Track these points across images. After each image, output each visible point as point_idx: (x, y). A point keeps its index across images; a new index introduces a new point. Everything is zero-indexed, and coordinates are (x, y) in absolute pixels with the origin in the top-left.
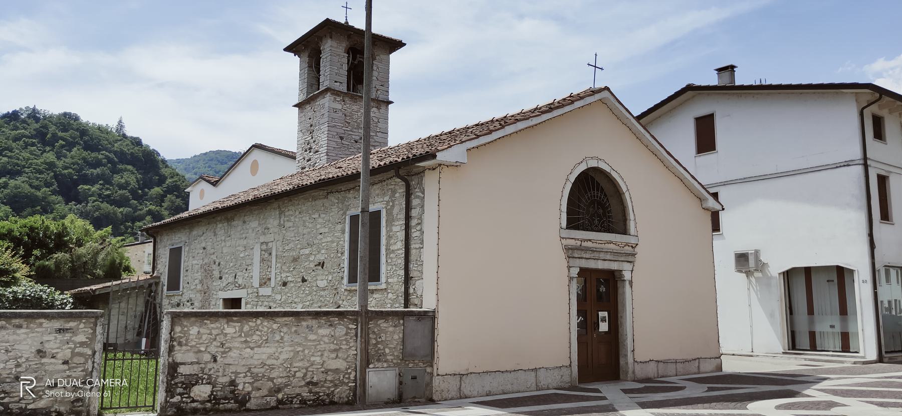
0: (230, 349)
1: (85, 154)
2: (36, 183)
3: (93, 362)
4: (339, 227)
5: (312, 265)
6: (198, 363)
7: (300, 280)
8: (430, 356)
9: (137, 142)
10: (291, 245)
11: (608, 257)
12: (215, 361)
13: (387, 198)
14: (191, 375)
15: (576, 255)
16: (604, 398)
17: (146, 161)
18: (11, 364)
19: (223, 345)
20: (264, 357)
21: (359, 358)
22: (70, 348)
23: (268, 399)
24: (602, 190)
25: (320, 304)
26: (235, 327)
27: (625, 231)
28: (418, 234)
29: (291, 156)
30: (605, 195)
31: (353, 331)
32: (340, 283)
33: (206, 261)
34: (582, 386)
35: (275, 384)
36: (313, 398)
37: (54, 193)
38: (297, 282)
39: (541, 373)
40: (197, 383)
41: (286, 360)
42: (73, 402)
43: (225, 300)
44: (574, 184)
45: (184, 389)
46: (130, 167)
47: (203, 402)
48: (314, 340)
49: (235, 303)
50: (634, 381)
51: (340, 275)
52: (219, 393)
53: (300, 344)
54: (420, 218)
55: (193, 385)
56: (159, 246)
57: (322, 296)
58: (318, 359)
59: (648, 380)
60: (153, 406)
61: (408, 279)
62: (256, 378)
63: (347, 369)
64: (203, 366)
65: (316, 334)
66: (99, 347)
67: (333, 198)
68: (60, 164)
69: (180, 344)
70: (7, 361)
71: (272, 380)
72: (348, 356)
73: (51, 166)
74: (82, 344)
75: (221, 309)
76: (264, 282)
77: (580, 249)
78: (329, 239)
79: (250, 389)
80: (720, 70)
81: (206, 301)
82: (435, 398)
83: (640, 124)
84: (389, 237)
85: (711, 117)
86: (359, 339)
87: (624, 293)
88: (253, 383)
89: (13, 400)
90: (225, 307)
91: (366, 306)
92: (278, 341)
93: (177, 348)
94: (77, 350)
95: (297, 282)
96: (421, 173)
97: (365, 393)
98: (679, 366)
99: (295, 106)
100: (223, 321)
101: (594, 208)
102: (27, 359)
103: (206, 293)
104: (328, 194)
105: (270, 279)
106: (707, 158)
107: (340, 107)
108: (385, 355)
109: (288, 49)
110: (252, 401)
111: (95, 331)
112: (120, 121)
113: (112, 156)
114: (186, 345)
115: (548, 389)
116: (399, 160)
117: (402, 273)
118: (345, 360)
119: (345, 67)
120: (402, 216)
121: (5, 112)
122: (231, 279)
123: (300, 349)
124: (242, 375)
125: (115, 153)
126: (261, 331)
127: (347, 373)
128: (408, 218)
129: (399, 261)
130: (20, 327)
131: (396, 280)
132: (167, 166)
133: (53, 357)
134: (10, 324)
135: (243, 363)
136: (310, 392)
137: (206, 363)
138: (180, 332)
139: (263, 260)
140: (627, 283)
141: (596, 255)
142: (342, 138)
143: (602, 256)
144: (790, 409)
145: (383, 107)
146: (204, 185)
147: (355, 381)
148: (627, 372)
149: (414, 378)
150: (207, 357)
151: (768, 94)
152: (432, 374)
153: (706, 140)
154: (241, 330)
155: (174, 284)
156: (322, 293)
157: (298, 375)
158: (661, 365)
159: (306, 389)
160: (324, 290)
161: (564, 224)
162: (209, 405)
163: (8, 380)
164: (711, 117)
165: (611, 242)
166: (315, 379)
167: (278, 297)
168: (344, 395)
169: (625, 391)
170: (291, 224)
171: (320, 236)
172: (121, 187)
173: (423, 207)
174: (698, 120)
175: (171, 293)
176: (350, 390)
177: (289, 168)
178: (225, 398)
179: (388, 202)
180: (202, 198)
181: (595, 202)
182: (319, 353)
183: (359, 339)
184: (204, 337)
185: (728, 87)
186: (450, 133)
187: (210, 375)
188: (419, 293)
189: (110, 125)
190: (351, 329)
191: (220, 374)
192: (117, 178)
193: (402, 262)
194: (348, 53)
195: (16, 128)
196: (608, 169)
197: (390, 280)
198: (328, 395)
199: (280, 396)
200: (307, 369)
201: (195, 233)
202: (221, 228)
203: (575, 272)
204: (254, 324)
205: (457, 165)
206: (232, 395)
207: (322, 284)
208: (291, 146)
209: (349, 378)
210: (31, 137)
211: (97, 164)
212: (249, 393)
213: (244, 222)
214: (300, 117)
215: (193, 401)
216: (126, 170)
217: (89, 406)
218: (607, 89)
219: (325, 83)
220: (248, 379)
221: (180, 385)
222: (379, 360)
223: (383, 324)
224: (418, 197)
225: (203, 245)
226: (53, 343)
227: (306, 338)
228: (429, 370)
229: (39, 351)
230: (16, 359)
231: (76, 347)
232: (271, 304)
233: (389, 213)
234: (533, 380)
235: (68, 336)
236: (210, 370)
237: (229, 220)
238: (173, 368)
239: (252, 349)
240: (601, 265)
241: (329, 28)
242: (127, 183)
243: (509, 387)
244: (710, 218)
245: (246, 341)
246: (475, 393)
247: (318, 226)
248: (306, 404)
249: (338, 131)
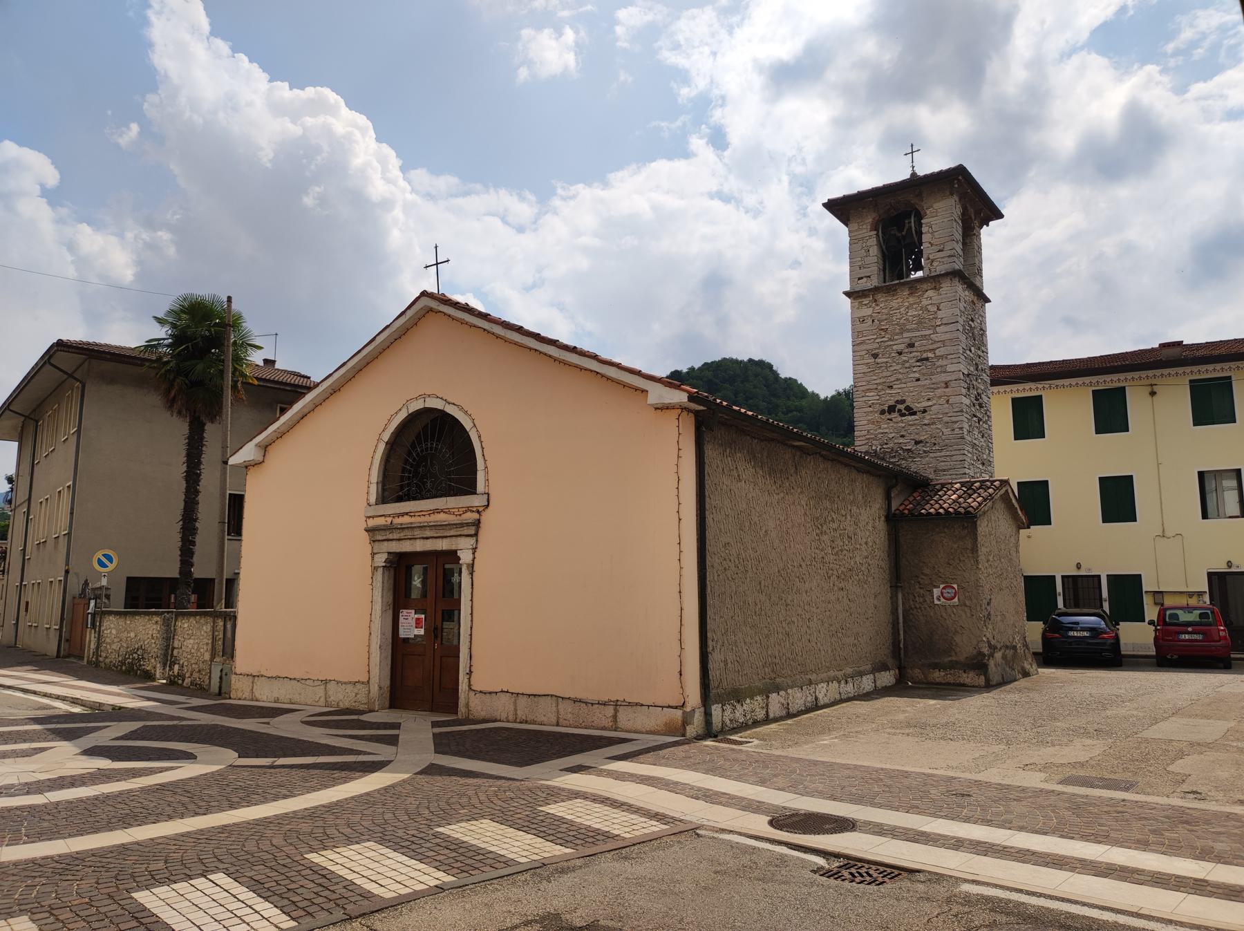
11: (428, 533)
39: (331, 686)
77: (390, 528)
107: (869, 311)
119: (874, 251)
141: (409, 533)
142: (875, 356)
143: (417, 533)
158: (522, 702)
161: (373, 499)
194: (876, 229)
203: (381, 560)
234: (322, 694)
243: (296, 698)
249: (869, 347)
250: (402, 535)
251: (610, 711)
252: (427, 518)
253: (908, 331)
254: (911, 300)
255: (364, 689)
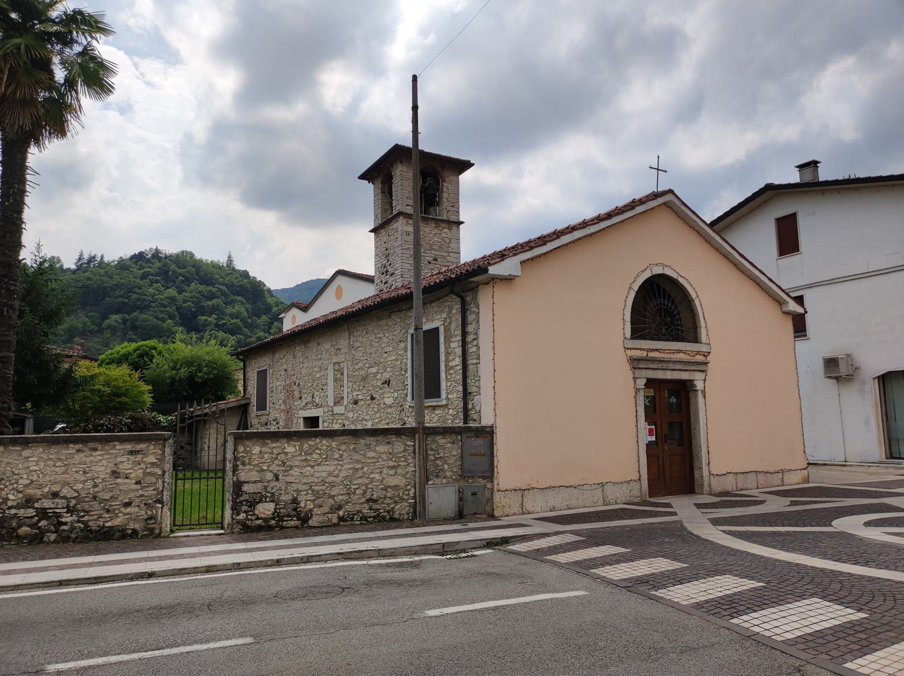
0: (291, 467)
1: (202, 288)
2: (162, 315)
3: (164, 482)
4: (402, 345)
5: (379, 383)
6: (260, 481)
7: (369, 398)
8: (490, 473)
9: (245, 274)
10: (360, 365)
11: (678, 367)
12: (277, 479)
13: (444, 315)
14: (254, 493)
15: (642, 366)
16: (675, 514)
17: (250, 290)
18: (89, 484)
19: (284, 463)
20: (324, 474)
21: (417, 475)
22: (142, 469)
23: (330, 515)
24: (670, 296)
25: (387, 421)
26: (295, 446)
27: (696, 339)
28: (474, 349)
29: (368, 279)
30: (673, 302)
31: (411, 448)
32: (405, 399)
33: (288, 382)
34: (653, 500)
35: (336, 502)
36: (373, 514)
37: (176, 324)
38: (366, 400)
39: (609, 489)
40: (260, 501)
41: (345, 478)
42: (146, 520)
43: (305, 418)
44: (637, 293)
45: (249, 506)
46: (239, 298)
47: (266, 520)
48: (373, 458)
49: (312, 421)
50: (710, 494)
51: (405, 392)
52: (282, 511)
53: (358, 461)
54: (476, 334)
55: (258, 503)
56: (248, 369)
57: (389, 413)
58: (377, 476)
59: (726, 494)
60: (222, 523)
61: (466, 395)
62: (317, 495)
63: (406, 486)
64: (266, 484)
65: (375, 451)
66: (168, 466)
67: (396, 318)
68: (180, 298)
69: (243, 464)
70: (86, 481)
71: (333, 497)
72: (407, 473)
73: (173, 300)
74: (153, 464)
75: (302, 428)
76: (338, 401)
78: (393, 358)
79: (312, 506)
80: (801, 167)
81: (289, 420)
82: (496, 514)
83: (714, 231)
84: (448, 354)
85: (793, 216)
86: (417, 455)
87: (697, 403)
88: (314, 500)
89: (91, 518)
90: (306, 425)
91: (423, 423)
92: (337, 459)
93: (241, 467)
94: (148, 471)
95: (366, 400)
96: (475, 289)
97: (425, 509)
98: (761, 477)
99: (371, 231)
100: (284, 441)
101: (661, 316)
102: (103, 480)
103: (288, 412)
104: (391, 313)
105: (343, 398)
106: (791, 260)
108: (443, 470)
109: (363, 177)
110: (315, 518)
111: (164, 452)
112: (230, 257)
113: (223, 288)
114: (250, 464)
115: (616, 503)
116: (453, 276)
117: (460, 388)
118: (404, 476)
120: (459, 332)
121: (132, 254)
122: (309, 399)
123: (359, 466)
124: (303, 493)
125: (227, 285)
126: (321, 450)
127: (406, 490)
128: (464, 334)
129: (458, 377)
130: (96, 450)
131: (455, 395)
132: (272, 296)
133: (127, 478)
134: (86, 447)
135: (304, 481)
136: (370, 509)
137: (268, 481)
138: (243, 452)
139: (336, 380)
140: (700, 393)
141: (665, 365)
143: (671, 366)
144: (882, 526)
145: (454, 228)
146: (295, 311)
147: (414, 497)
148: (702, 486)
149: (474, 494)
150: (269, 476)
151: (857, 189)
152: (492, 489)
153: (788, 241)
154: (301, 449)
155: (262, 405)
156: (389, 410)
157: (358, 492)
158: (740, 477)
159: (366, 506)
160: (391, 407)
161: (628, 334)
162: (273, 522)
163: (87, 499)
164: (793, 216)
165: (680, 351)
166: (375, 497)
167: (350, 415)
168: (404, 512)
169: (699, 506)
170: (359, 344)
171: (385, 355)
172: (233, 316)
173: (478, 322)
174: (780, 221)
175: (260, 413)
176: (410, 506)
177: (367, 292)
178: (288, 516)
179: (445, 321)
180: (293, 320)
181: (662, 309)
182: (378, 470)
183: (417, 455)
184: (266, 456)
185: (812, 185)
186: (513, 248)
187: (273, 494)
188: (477, 408)
189: (221, 261)
190: (409, 446)
191: (283, 492)
192: (230, 310)
193: (459, 377)
195: (141, 268)
196: (674, 275)
197: (450, 396)
198: (388, 512)
199: (341, 513)
200: (366, 485)
201: (277, 356)
202: (299, 351)
203: (641, 383)
204: (313, 443)
205: (508, 279)
206: (294, 513)
207: (389, 401)
208: (369, 269)
209: (408, 494)
210: (157, 275)
211: (211, 296)
212: (311, 510)
213: (319, 344)
214: (376, 242)
215: (258, 518)
216: (236, 301)
217: (161, 523)
218: (671, 191)
219: (398, 207)
220: (310, 497)
221: (244, 503)
222: (437, 476)
223: (441, 440)
224: (473, 312)
225: (285, 367)
226: (126, 464)
227: (364, 455)
228: (489, 486)
229: (114, 472)
230: (93, 479)
231: (147, 468)
232: (345, 422)
233: (447, 330)
234: (600, 496)
235: (139, 457)
236: (273, 488)
237: (306, 342)
238: (238, 486)
239: (312, 467)
240: (669, 375)
241: (398, 154)
242: (239, 313)
243: (574, 502)
244: (791, 323)
245: (306, 460)
246: (539, 509)
247: (384, 345)
248: (367, 521)
250: (660, 366)
251: (780, 475)
252: (671, 356)
253: (435, 250)
254: (436, 231)
255: (637, 486)
